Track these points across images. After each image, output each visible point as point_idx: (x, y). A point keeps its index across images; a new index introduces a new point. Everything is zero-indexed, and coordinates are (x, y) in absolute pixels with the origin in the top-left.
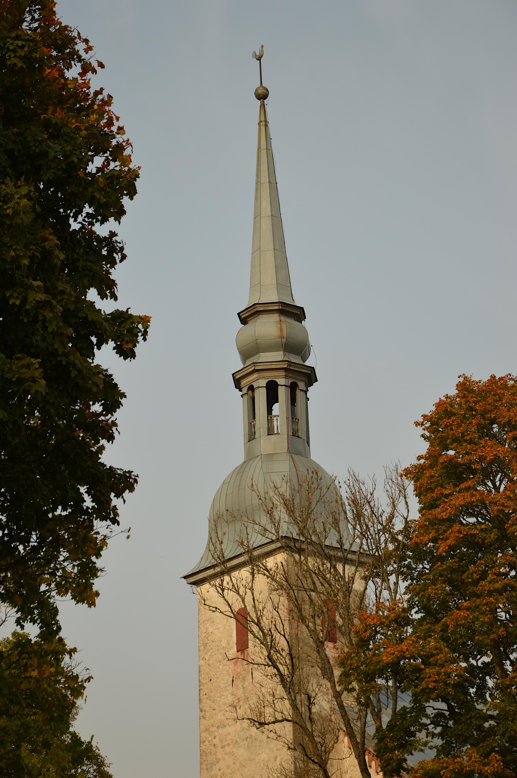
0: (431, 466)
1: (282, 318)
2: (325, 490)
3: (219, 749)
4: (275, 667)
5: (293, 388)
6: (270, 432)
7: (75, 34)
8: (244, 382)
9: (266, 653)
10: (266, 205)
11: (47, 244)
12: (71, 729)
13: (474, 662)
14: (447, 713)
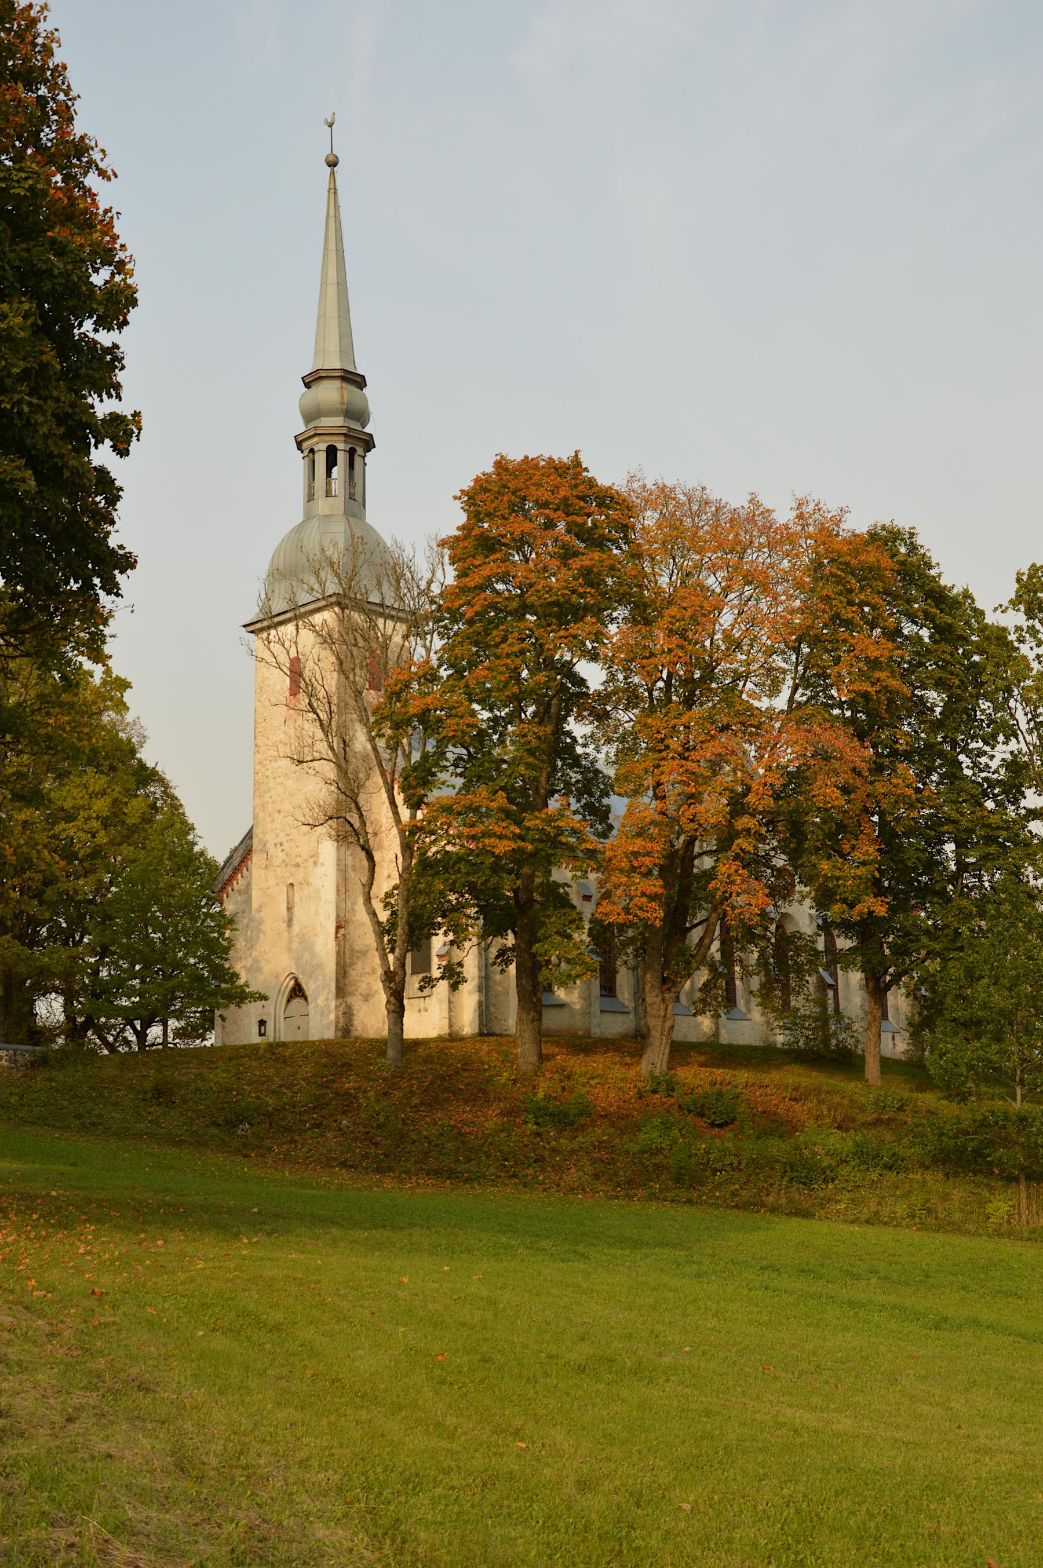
0: (465, 538)
1: (344, 385)
2: (368, 554)
3: (271, 780)
4: (315, 713)
5: (352, 452)
6: (328, 494)
7: (93, 144)
8: (306, 445)
9: (307, 701)
10: (332, 272)
11: (44, 357)
12: (138, 756)
13: (498, 714)
14: (466, 757)
